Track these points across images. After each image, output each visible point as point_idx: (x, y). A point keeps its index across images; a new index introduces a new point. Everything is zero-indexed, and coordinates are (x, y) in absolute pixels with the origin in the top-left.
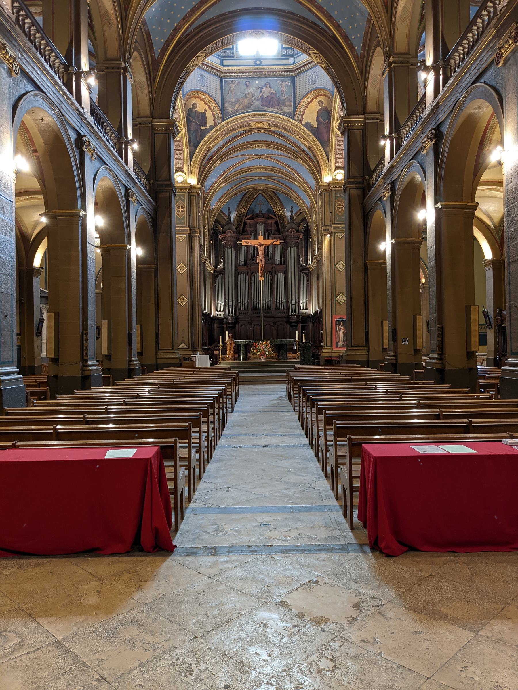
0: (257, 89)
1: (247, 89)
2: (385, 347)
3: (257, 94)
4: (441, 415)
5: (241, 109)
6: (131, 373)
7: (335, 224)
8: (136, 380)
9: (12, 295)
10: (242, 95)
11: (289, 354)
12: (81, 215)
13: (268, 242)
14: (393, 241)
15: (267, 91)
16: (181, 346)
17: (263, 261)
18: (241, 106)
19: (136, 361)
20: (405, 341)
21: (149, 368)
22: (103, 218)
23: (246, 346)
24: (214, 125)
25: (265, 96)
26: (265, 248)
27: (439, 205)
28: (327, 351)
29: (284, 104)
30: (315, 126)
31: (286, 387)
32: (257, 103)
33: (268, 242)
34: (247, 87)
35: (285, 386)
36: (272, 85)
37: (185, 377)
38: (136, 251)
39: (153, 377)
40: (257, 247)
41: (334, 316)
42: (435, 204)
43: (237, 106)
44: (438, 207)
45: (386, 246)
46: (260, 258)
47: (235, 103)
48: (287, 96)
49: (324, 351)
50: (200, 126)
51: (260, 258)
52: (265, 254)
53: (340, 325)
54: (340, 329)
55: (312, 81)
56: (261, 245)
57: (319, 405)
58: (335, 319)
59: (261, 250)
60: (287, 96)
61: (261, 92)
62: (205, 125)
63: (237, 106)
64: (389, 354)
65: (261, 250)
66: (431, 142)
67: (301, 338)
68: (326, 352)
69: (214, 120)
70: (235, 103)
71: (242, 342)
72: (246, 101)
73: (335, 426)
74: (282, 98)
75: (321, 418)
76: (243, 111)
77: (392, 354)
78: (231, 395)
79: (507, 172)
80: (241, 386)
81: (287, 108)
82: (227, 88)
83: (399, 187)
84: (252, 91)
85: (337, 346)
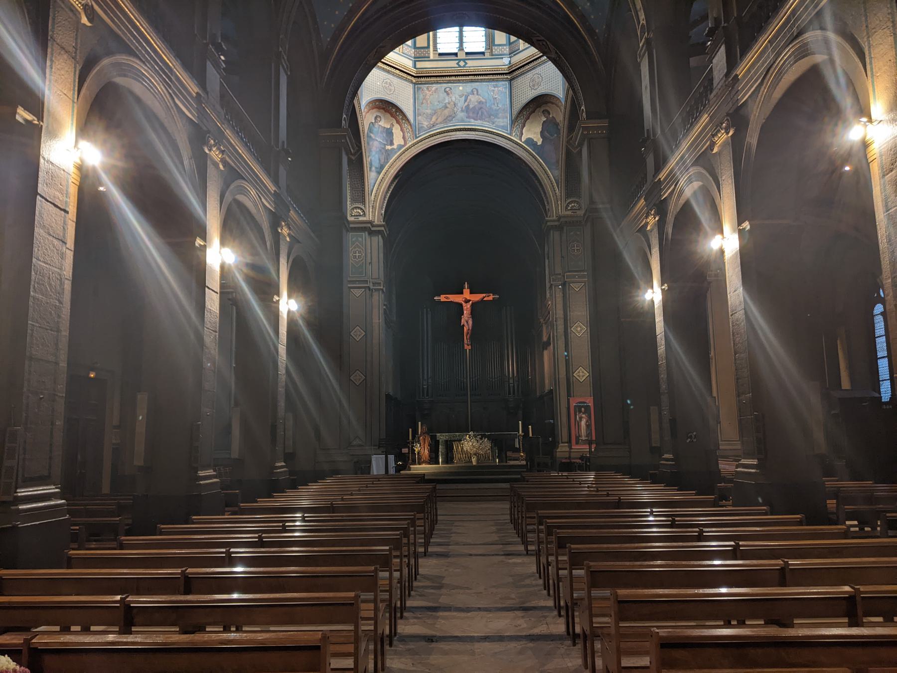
0: (461, 96)
1: (447, 98)
2: (654, 445)
3: (461, 104)
4: (858, 598)
5: (441, 123)
6: (273, 487)
7: (569, 271)
8: (279, 501)
9: (57, 363)
10: (441, 105)
11: (509, 454)
12: (197, 245)
13: (477, 297)
14: (665, 287)
15: (473, 99)
16: (355, 443)
17: (470, 322)
18: (440, 120)
19: (282, 467)
20: (691, 437)
21: (297, 481)
22: (233, 252)
23: (446, 441)
24: (403, 143)
25: (471, 106)
26: (473, 304)
27: (746, 225)
28: (564, 449)
29: (496, 116)
30: (539, 143)
31: (508, 506)
32: (461, 115)
33: (477, 297)
34: (448, 94)
35: (507, 506)
36: (480, 92)
37: (352, 494)
38: (289, 305)
39: (305, 498)
40: (461, 305)
41: (571, 399)
42: (739, 224)
43: (434, 119)
44: (744, 229)
45: (653, 295)
46: (467, 320)
47: (432, 115)
48: (500, 106)
49: (559, 450)
50: (385, 145)
51: (467, 320)
52: (473, 313)
53: (580, 411)
54: (581, 418)
55: (534, 85)
56: (467, 301)
57: (558, 533)
58: (573, 404)
59: (467, 308)
60: (500, 106)
61: (465, 101)
62: (392, 143)
63: (434, 119)
64: (666, 456)
65: (467, 308)
66: (728, 133)
67: (525, 430)
68: (562, 450)
69: (404, 138)
70: (432, 115)
71: (442, 437)
72: (447, 112)
73: (570, 551)
74: (494, 107)
75: (579, 572)
76: (442, 125)
77: (671, 456)
78: (424, 526)
79: (881, 156)
80: (440, 505)
81: (501, 120)
82: (421, 96)
83: (673, 209)
84: (454, 99)
85: (577, 443)
